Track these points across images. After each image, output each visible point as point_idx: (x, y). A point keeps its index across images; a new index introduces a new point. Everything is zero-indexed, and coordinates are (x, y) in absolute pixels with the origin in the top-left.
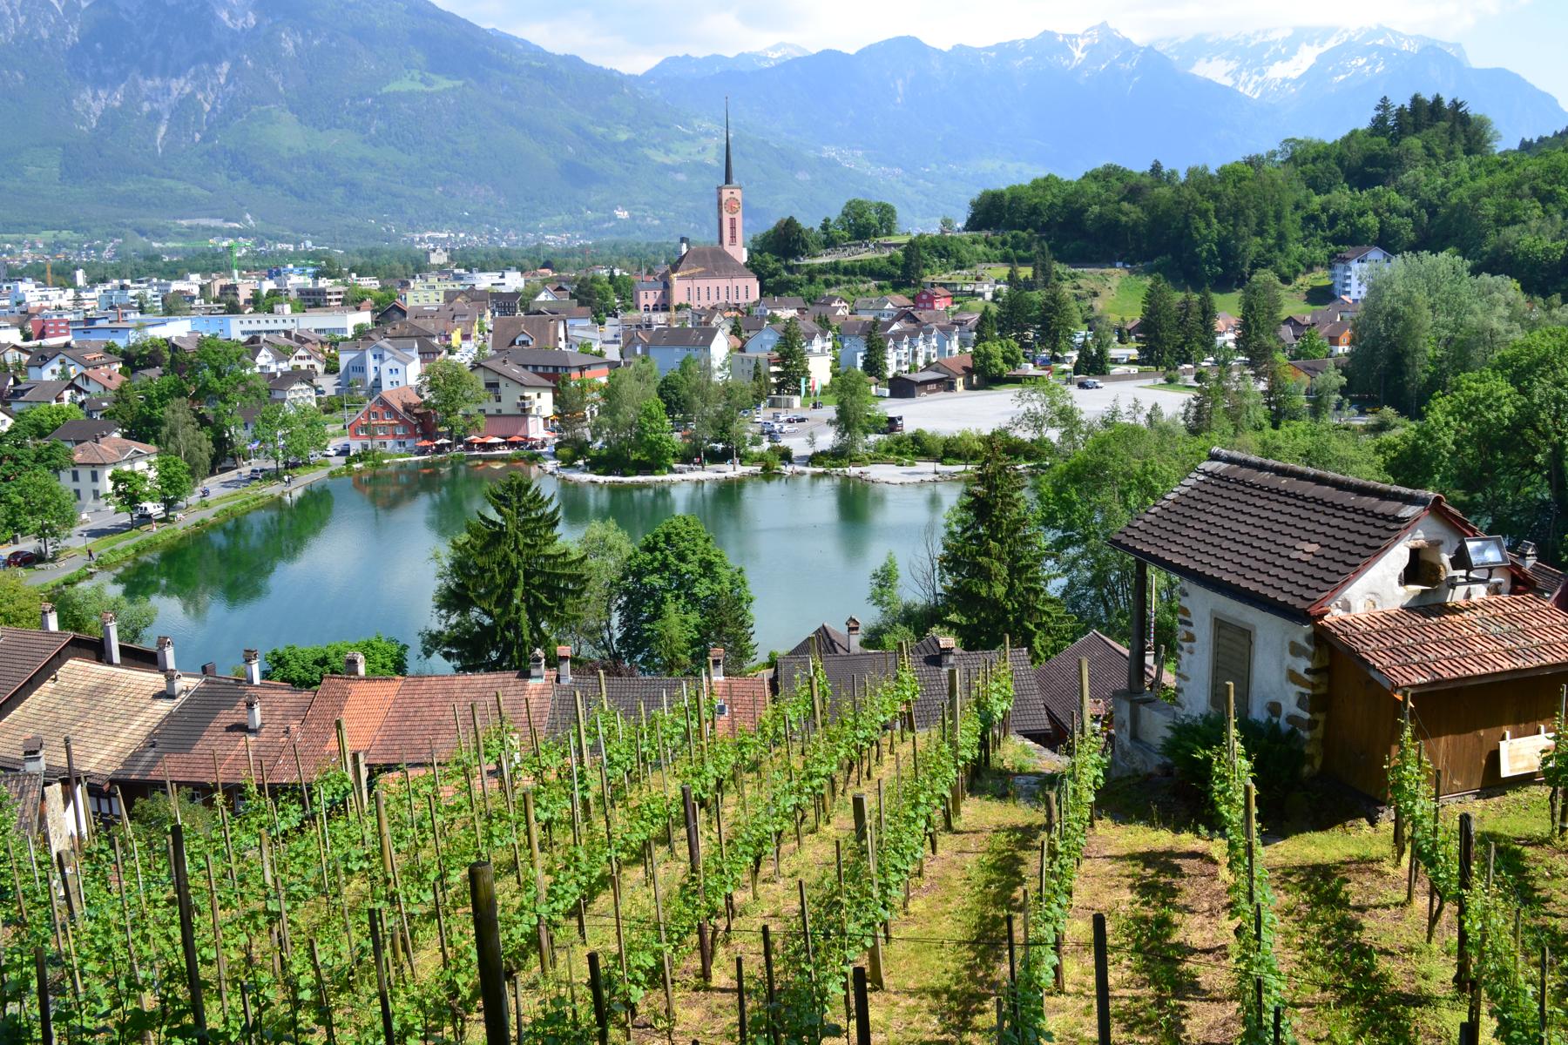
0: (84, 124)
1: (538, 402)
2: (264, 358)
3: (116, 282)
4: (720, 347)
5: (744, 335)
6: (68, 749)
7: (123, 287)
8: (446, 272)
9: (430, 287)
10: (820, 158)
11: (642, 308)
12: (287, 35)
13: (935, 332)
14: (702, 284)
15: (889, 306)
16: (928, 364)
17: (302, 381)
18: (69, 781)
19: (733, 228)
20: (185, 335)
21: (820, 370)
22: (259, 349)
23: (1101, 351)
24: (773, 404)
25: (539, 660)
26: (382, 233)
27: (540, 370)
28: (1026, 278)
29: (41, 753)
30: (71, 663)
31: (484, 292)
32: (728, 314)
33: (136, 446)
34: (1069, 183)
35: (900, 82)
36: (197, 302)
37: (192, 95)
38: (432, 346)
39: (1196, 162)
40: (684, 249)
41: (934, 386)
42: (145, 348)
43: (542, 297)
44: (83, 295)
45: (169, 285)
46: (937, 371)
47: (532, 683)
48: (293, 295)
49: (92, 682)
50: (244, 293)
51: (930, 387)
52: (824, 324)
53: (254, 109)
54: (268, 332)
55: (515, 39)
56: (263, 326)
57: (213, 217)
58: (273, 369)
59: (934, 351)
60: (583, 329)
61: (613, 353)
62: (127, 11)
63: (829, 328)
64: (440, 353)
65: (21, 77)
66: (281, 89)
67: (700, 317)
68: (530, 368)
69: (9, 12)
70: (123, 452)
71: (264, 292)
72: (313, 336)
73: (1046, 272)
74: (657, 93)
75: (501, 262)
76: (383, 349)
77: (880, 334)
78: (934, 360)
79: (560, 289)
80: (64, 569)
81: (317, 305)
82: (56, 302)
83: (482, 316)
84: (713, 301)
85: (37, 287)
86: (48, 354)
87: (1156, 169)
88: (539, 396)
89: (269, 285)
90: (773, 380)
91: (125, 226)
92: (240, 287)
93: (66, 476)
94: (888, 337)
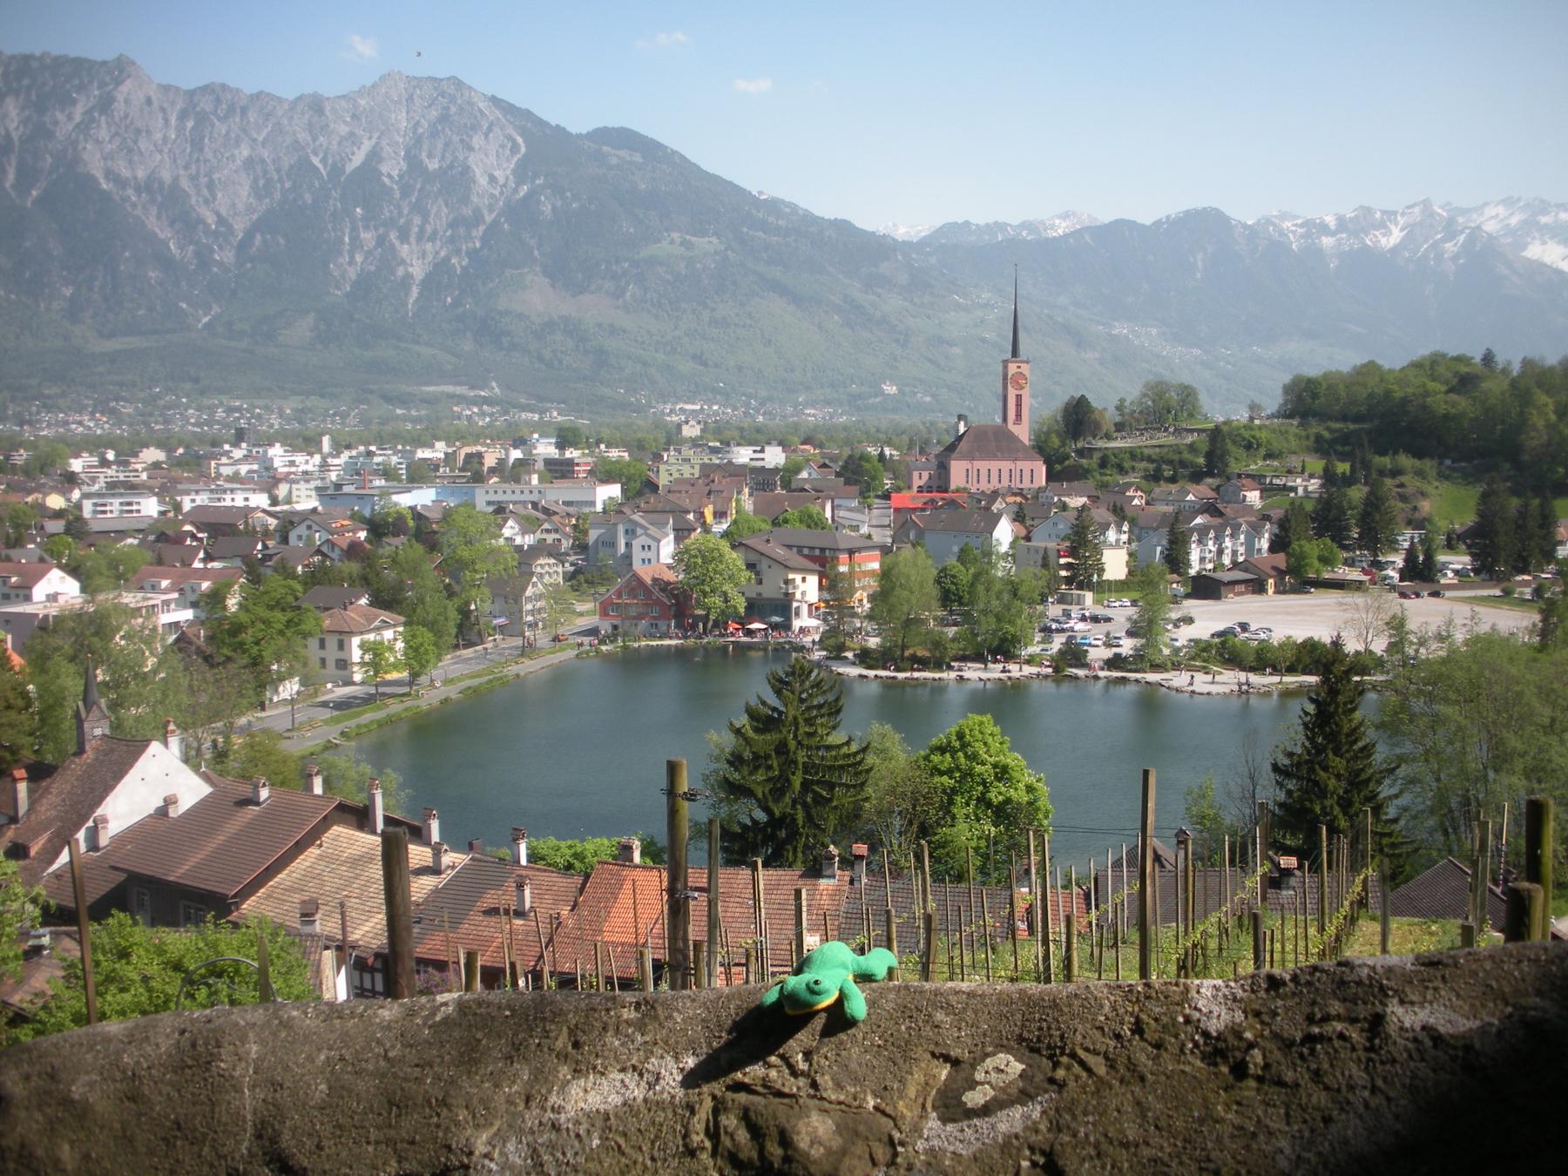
0: (339, 289)
1: (801, 587)
2: (510, 529)
3: (362, 448)
4: (1004, 533)
5: (1029, 522)
6: (343, 914)
7: (370, 454)
8: (700, 445)
9: (683, 460)
10: (1111, 335)
11: (915, 489)
12: (546, 198)
13: (1244, 528)
14: (983, 465)
15: (1190, 497)
16: (1235, 565)
17: (550, 555)
18: (342, 948)
19: (1019, 405)
20: (430, 504)
21: (1115, 564)
22: (505, 520)
23: (1429, 557)
24: (1062, 600)
25: (832, 857)
26: (631, 404)
27: (806, 551)
28: (1344, 473)
29: (318, 917)
30: (337, 830)
31: (744, 466)
32: (1010, 499)
33: (385, 615)
34: (1391, 371)
35: (1200, 256)
36: (441, 470)
37: (447, 259)
38: (687, 521)
39: (1532, 353)
40: (962, 429)
41: (1242, 588)
42: (388, 514)
43: (804, 475)
44: (330, 460)
45: (414, 452)
46: (1246, 570)
47: (824, 883)
48: (540, 465)
49: (355, 851)
50: (490, 461)
51: (1238, 588)
52: (1120, 513)
53: (508, 272)
54: (515, 503)
55: (783, 202)
56: (508, 497)
57: (460, 384)
58: (518, 541)
59: (1242, 550)
60: (851, 510)
61: (884, 537)
62: (390, 176)
63: (1124, 519)
64: (695, 530)
65: (282, 241)
66: (536, 253)
67: (979, 501)
68: (795, 550)
69: (276, 178)
70: (370, 621)
71: (511, 461)
72: (561, 509)
73: (1366, 465)
74: (933, 260)
75: (758, 438)
76: (636, 524)
77: (1182, 527)
78: (1241, 559)
79: (824, 466)
80: (310, 739)
81: (563, 477)
82: (303, 468)
83: (739, 493)
84: (994, 484)
85: (286, 451)
86: (296, 519)
87: (1488, 359)
88: (804, 580)
89: (516, 454)
90: (1063, 573)
91: (372, 392)
92: (486, 455)
93: (313, 643)
94: (1192, 530)
